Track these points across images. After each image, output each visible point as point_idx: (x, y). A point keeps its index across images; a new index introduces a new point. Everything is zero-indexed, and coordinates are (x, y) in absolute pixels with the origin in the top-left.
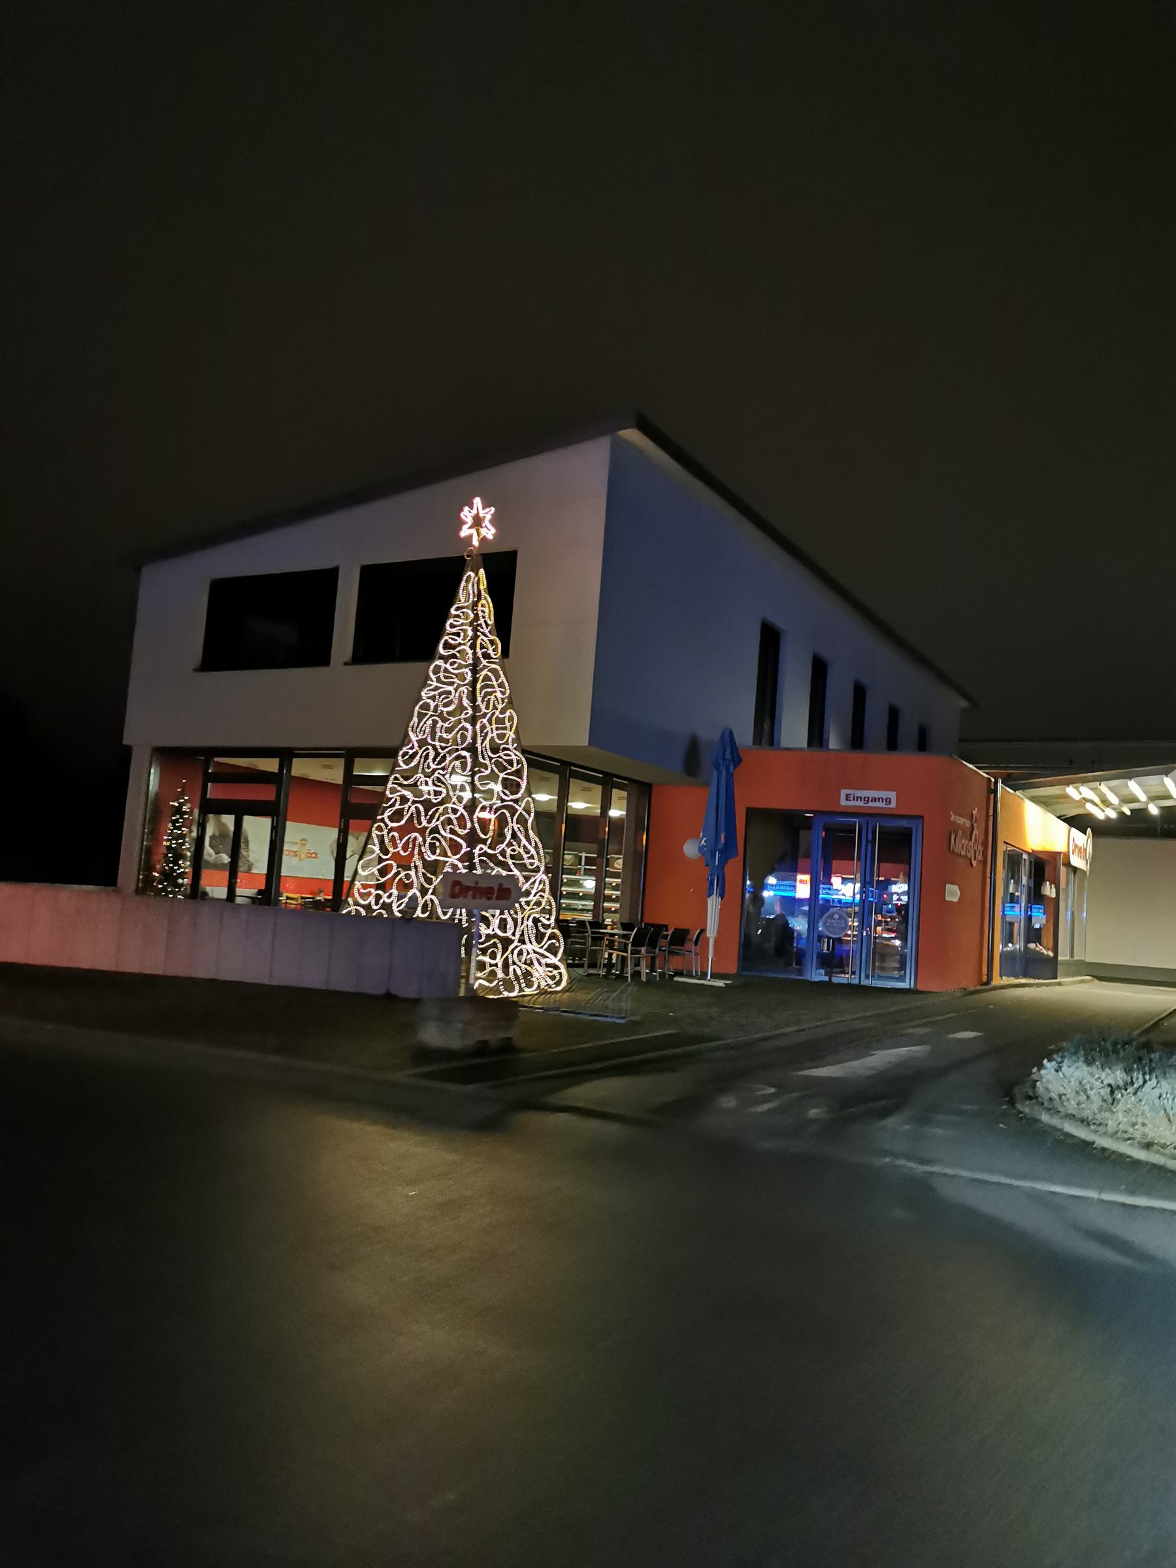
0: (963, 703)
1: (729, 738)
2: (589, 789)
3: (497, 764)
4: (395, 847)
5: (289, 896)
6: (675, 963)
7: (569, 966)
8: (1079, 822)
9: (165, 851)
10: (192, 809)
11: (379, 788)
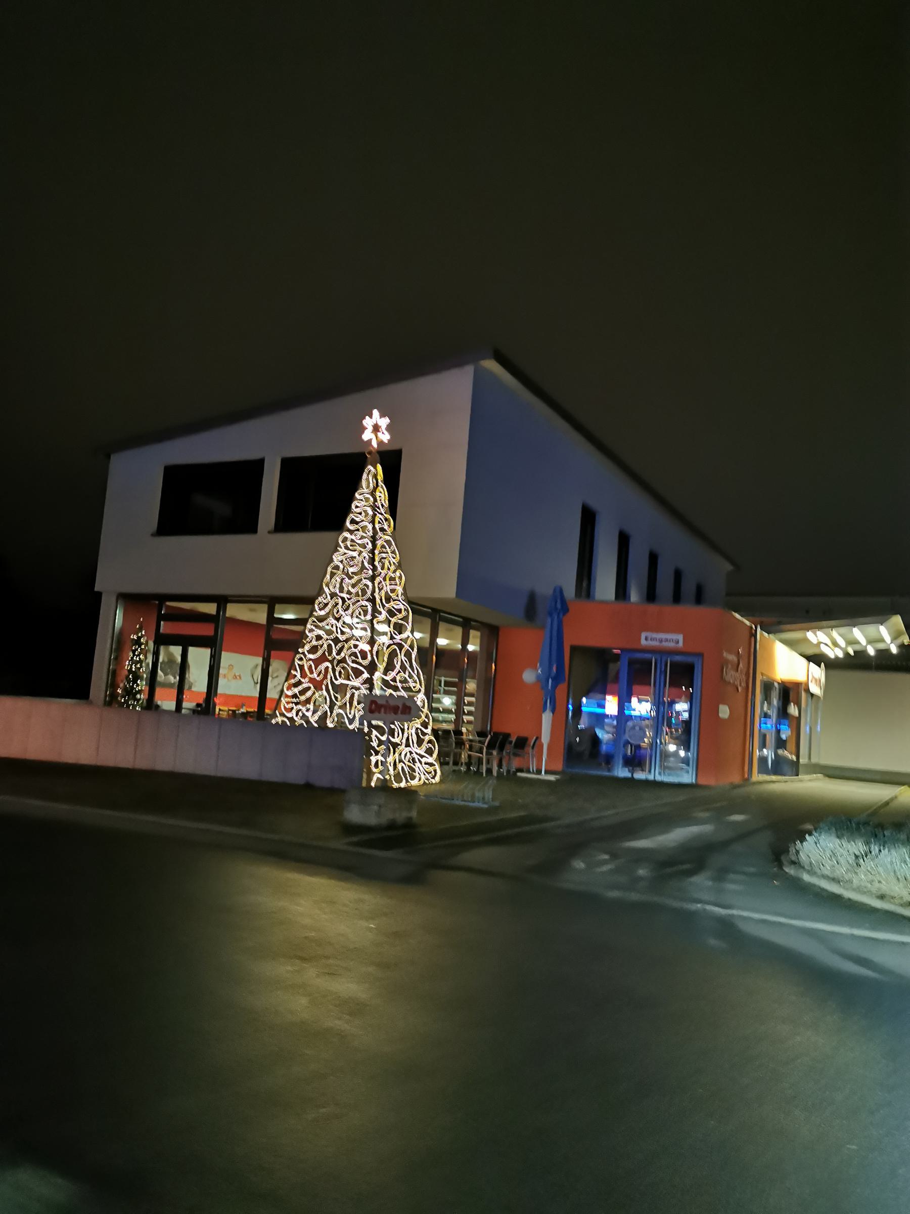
0: (729, 567)
1: (559, 593)
2: (451, 630)
4: (312, 672)
5: (221, 708)
6: (515, 763)
8: (816, 659)
9: (127, 673)
10: (147, 642)
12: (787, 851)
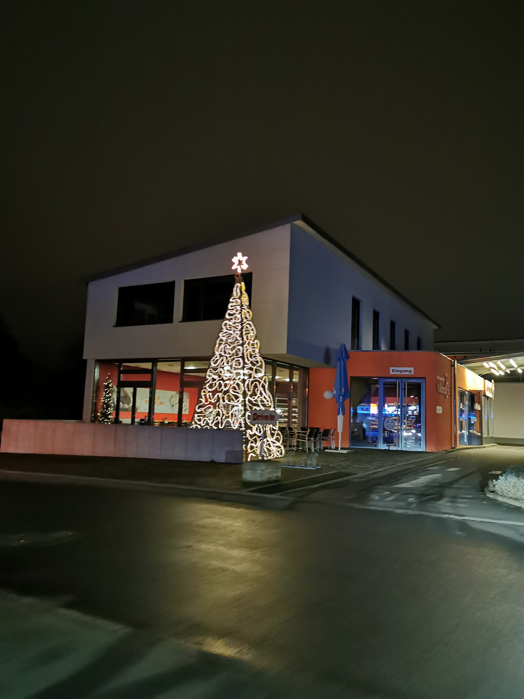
0: (436, 327)
1: (344, 347)
2: (282, 371)
3: (251, 362)
5: (157, 421)
6: (324, 444)
7: (285, 446)
8: (488, 377)
9: (102, 404)
11: (202, 375)
12: (487, 485)
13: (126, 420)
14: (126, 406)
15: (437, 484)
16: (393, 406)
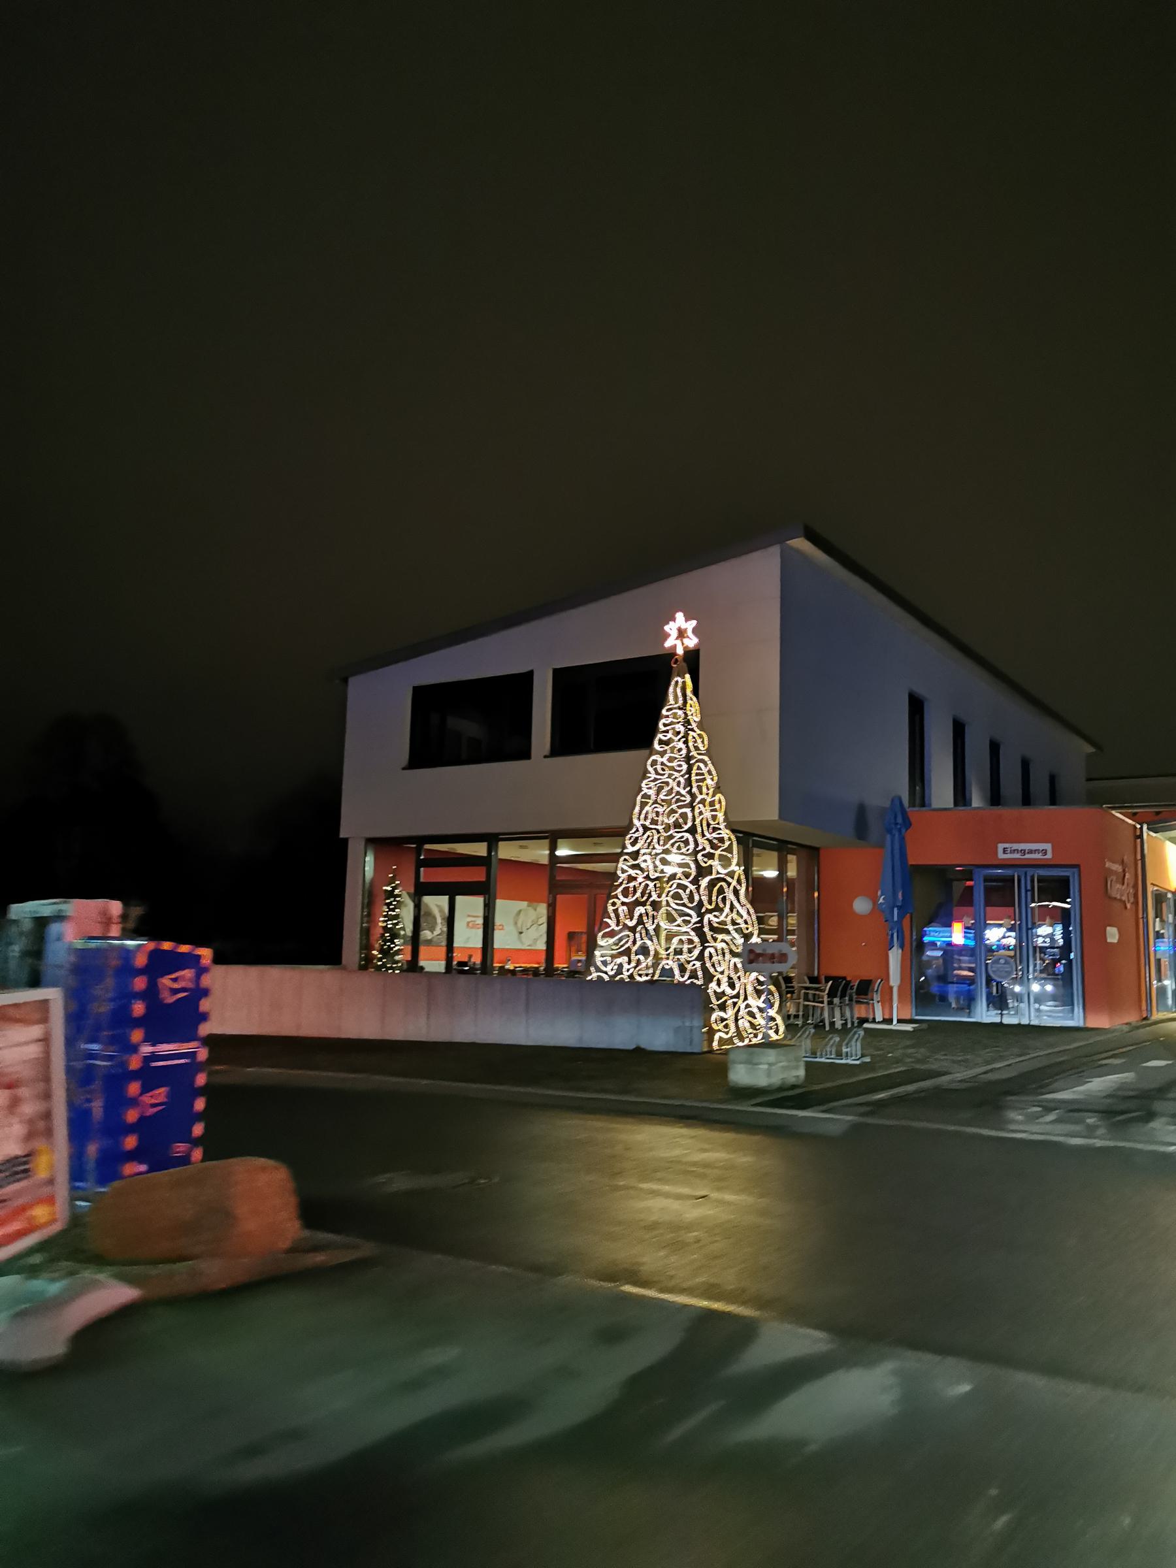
0: (1090, 749)
6: (860, 1011)
9: (381, 931)
13: (433, 964)
14: (434, 933)
15: (1131, 1093)
16: (1000, 926)
